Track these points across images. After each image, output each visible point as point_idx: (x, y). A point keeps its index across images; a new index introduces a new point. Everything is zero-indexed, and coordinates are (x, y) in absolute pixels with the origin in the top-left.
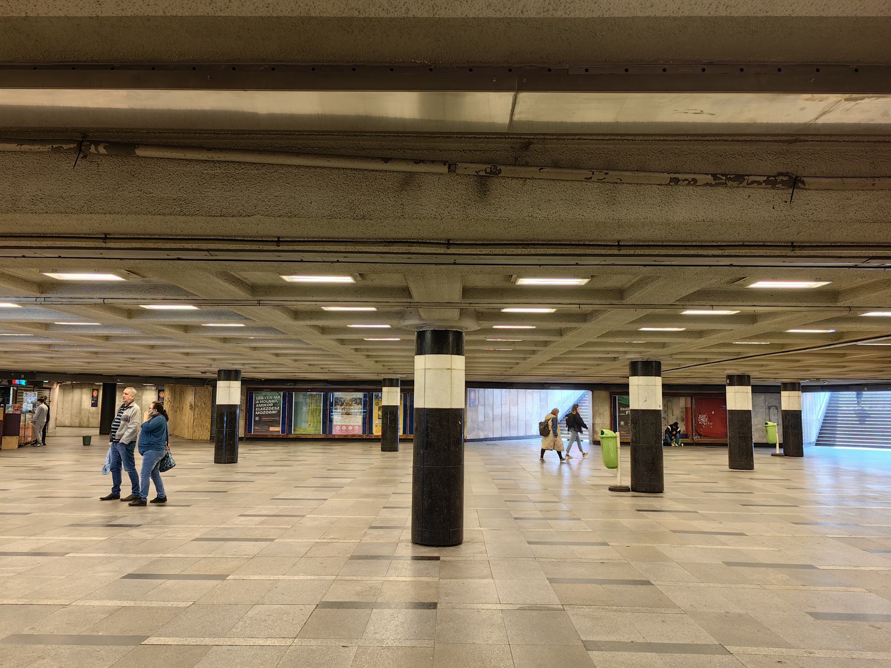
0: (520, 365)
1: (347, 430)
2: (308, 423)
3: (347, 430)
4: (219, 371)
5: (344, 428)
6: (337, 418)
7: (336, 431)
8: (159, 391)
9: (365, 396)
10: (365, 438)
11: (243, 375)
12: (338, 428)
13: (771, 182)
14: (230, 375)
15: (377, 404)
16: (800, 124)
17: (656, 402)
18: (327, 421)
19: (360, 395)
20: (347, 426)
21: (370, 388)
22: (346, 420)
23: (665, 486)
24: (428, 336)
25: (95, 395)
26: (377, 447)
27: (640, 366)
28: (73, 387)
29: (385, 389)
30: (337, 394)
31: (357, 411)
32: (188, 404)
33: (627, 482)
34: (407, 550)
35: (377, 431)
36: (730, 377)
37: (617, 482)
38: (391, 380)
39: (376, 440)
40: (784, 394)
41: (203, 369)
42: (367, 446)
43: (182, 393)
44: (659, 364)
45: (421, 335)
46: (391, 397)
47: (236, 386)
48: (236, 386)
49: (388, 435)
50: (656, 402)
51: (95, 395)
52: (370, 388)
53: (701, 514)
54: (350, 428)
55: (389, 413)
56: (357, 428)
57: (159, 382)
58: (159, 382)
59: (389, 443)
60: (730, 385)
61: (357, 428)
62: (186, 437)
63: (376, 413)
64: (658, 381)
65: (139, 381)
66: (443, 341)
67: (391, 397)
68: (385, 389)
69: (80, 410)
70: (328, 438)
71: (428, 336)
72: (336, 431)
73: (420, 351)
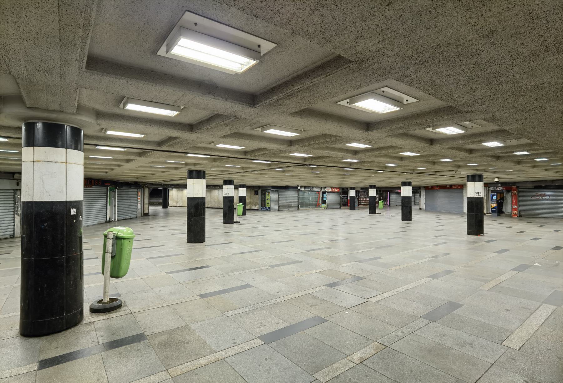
0: (114, 171)
14: (405, 184)
16: (374, 113)
27: (194, 173)
44: (204, 172)
45: (30, 127)
53: (199, 261)
54: (269, 201)
63: (18, 204)
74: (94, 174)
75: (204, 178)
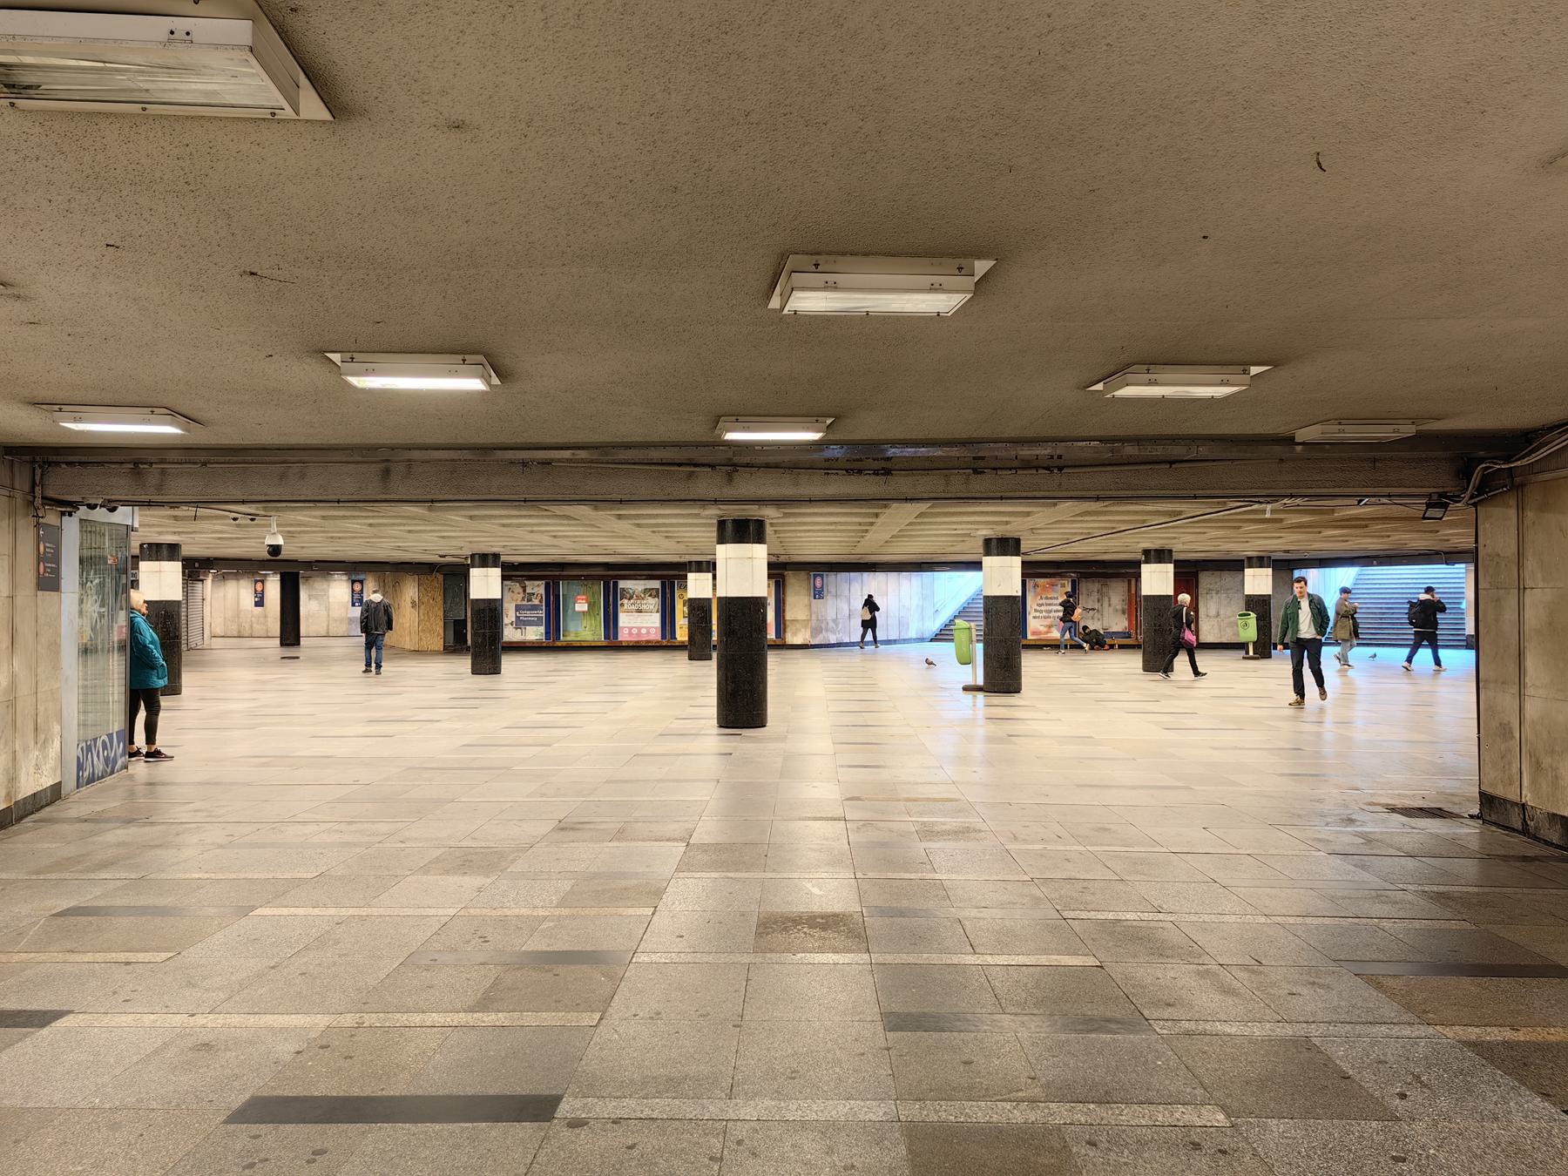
1: (639, 634)
2: (582, 622)
3: (639, 634)
4: (473, 556)
5: (635, 631)
6: (625, 620)
7: (624, 636)
8: (353, 582)
9: (663, 585)
10: (665, 644)
11: (503, 558)
12: (626, 631)
13: (876, 473)
15: (681, 596)
17: (1167, 588)
18: (611, 622)
19: (656, 584)
20: (639, 629)
21: (669, 575)
22: (641, 620)
23: (1024, 680)
24: (729, 526)
25: (259, 588)
26: (683, 656)
28: (224, 577)
29: (691, 576)
30: (622, 584)
31: (653, 603)
32: (409, 600)
33: (980, 681)
34: (716, 730)
35: (682, 635)
36: (1146, 552)
37: (970, 682)
38: (699, 563)
39: (681, 647)
40: (692, 577)
41: (200, 525)
42: (668, 655)
43: (397, 584)
44: (1018, 541)
46: (698, 586)
47: (174, 569)
48: (174, 569)
49: (698, 638)
50: (1167, 588)
51: (259, 588)
52: (669, 575)
54: (644, 631)
55: (699, 609)
56: (653, 631)
57: (355, 569)
58: (355, 569)
59: (697, 649)
60: (1147, 562)
61: (653, 631)
62: (408, 647)
63: (681, 611)
64: (1016, 562)
65: (326, 567)
66: (743, 531)
67: (698, 586)
68: (691, 576)
69: (238, 613)
70: (612, 645)
71: (729, 526)
72: (624, 636)
73: (721, 541)
74: (774, 559)
75: (1018, 555)
